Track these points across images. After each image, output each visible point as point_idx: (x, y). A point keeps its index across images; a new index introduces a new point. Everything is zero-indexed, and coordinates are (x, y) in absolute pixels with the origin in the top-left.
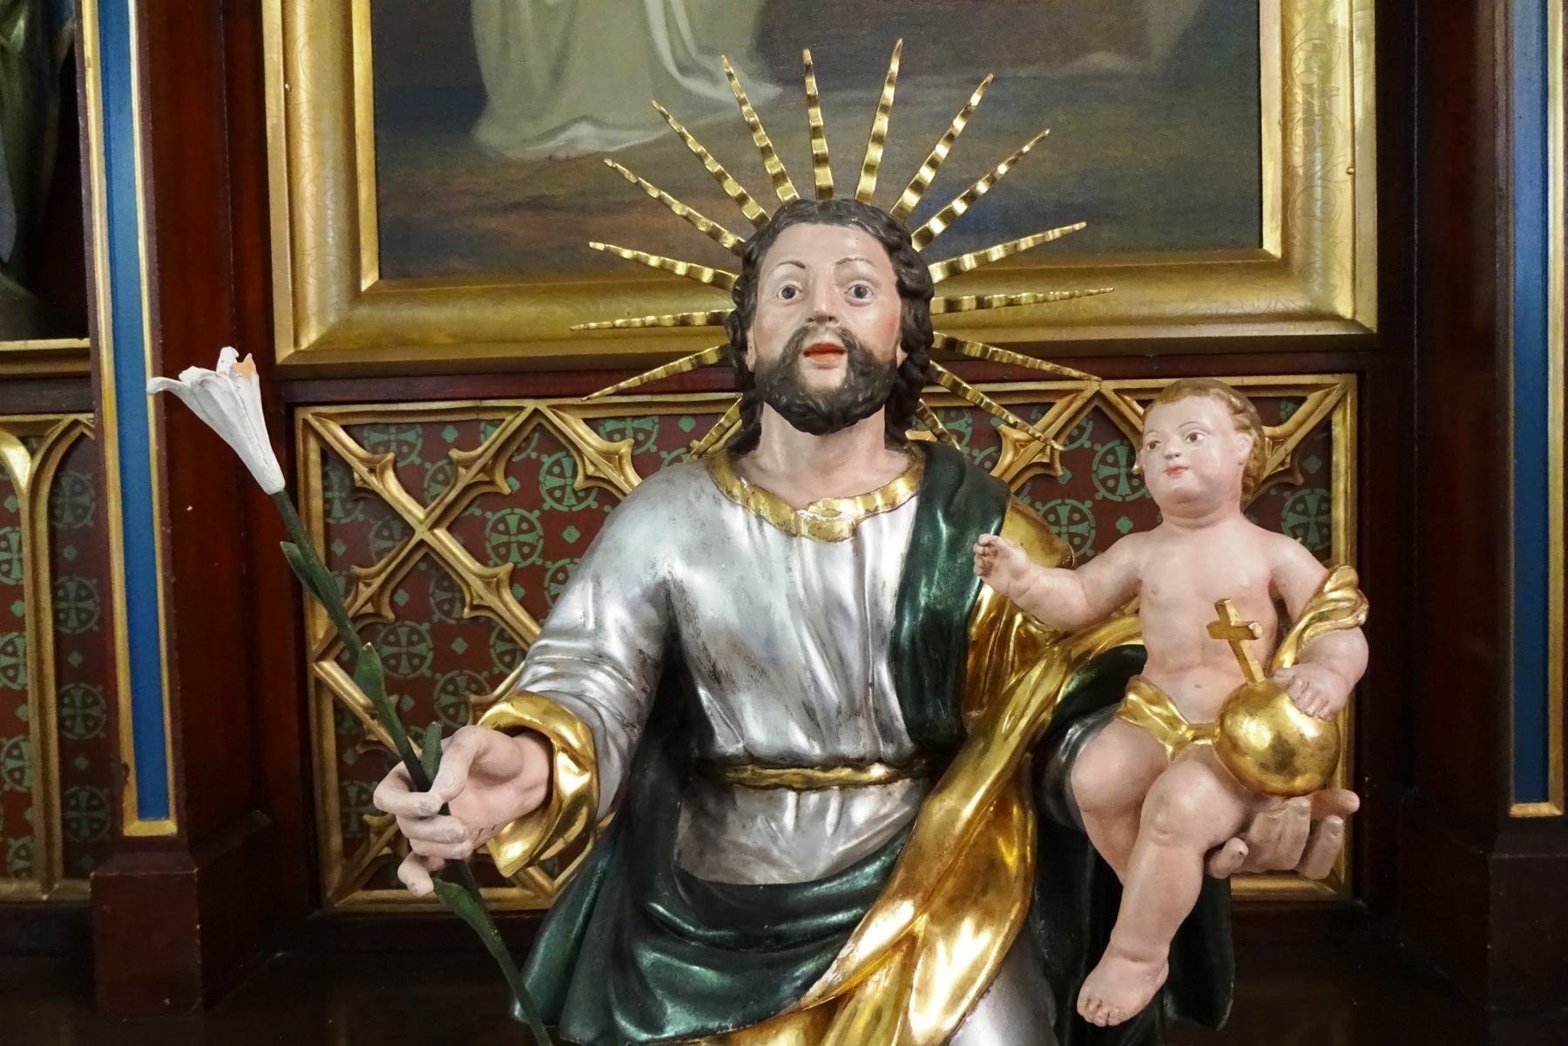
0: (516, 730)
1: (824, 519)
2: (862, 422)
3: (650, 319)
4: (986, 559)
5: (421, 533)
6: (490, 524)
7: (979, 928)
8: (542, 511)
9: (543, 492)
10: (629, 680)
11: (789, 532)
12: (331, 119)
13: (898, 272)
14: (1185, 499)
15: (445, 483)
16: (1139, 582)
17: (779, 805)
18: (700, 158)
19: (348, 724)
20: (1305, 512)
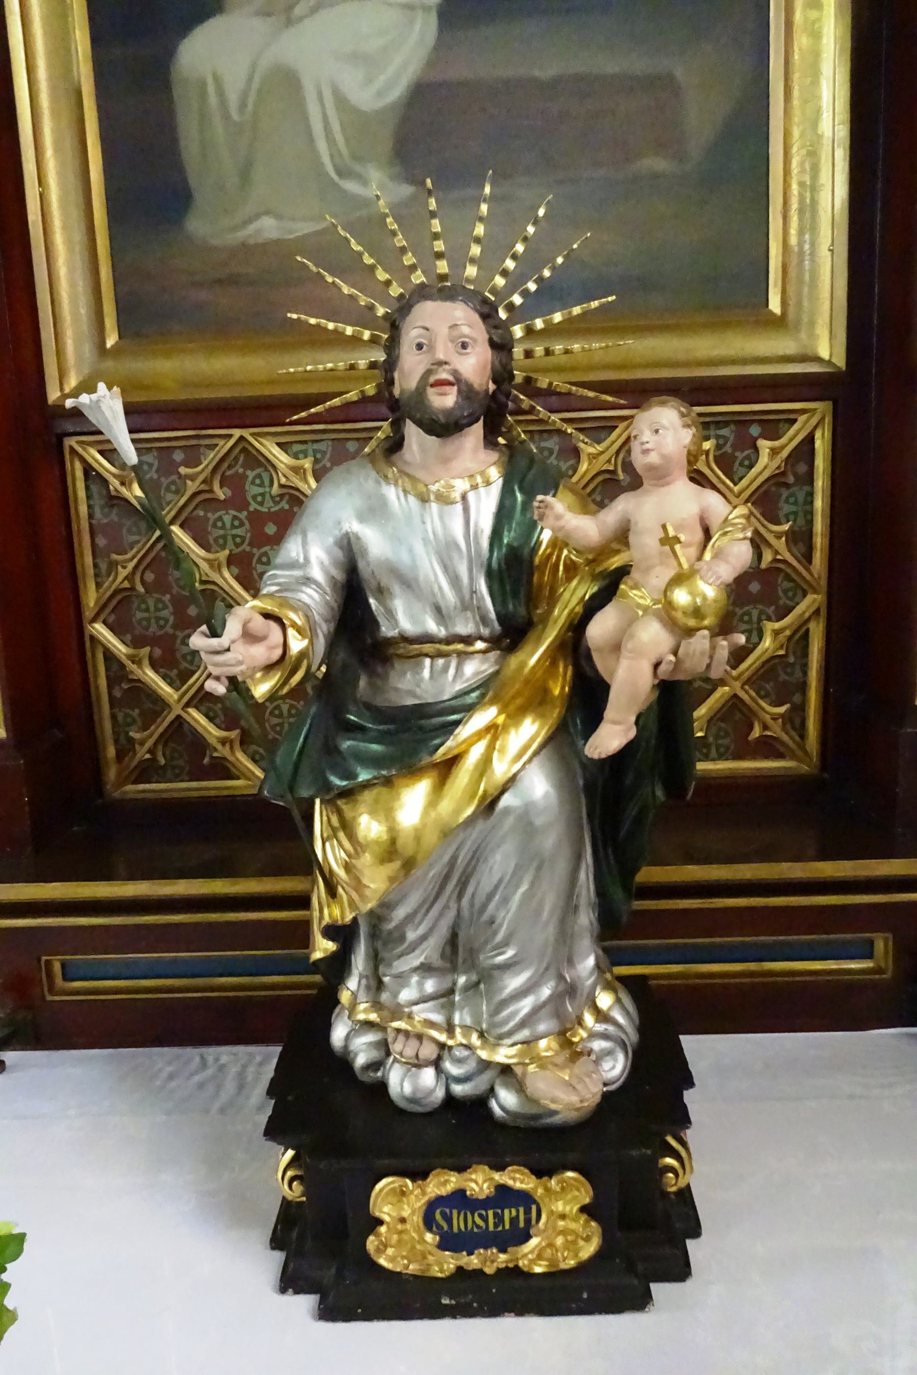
0: (267, 616)
1: (444, 490)
2: (467, 430)
3: (330, 365)
4: (541, 510)
6: (211, 522)
7: (534, 722)
8: (249, 512)
9: (250, 499)
10: (327, 594)
11: (424, 500)
12: (76, 214)
13: (488, 332)
14: (651, 468)
15: (177, 492)
16: (629, 521)
17: (421, 666)
18: (360, 254)
19: (115, 667)
20: (796, 503)
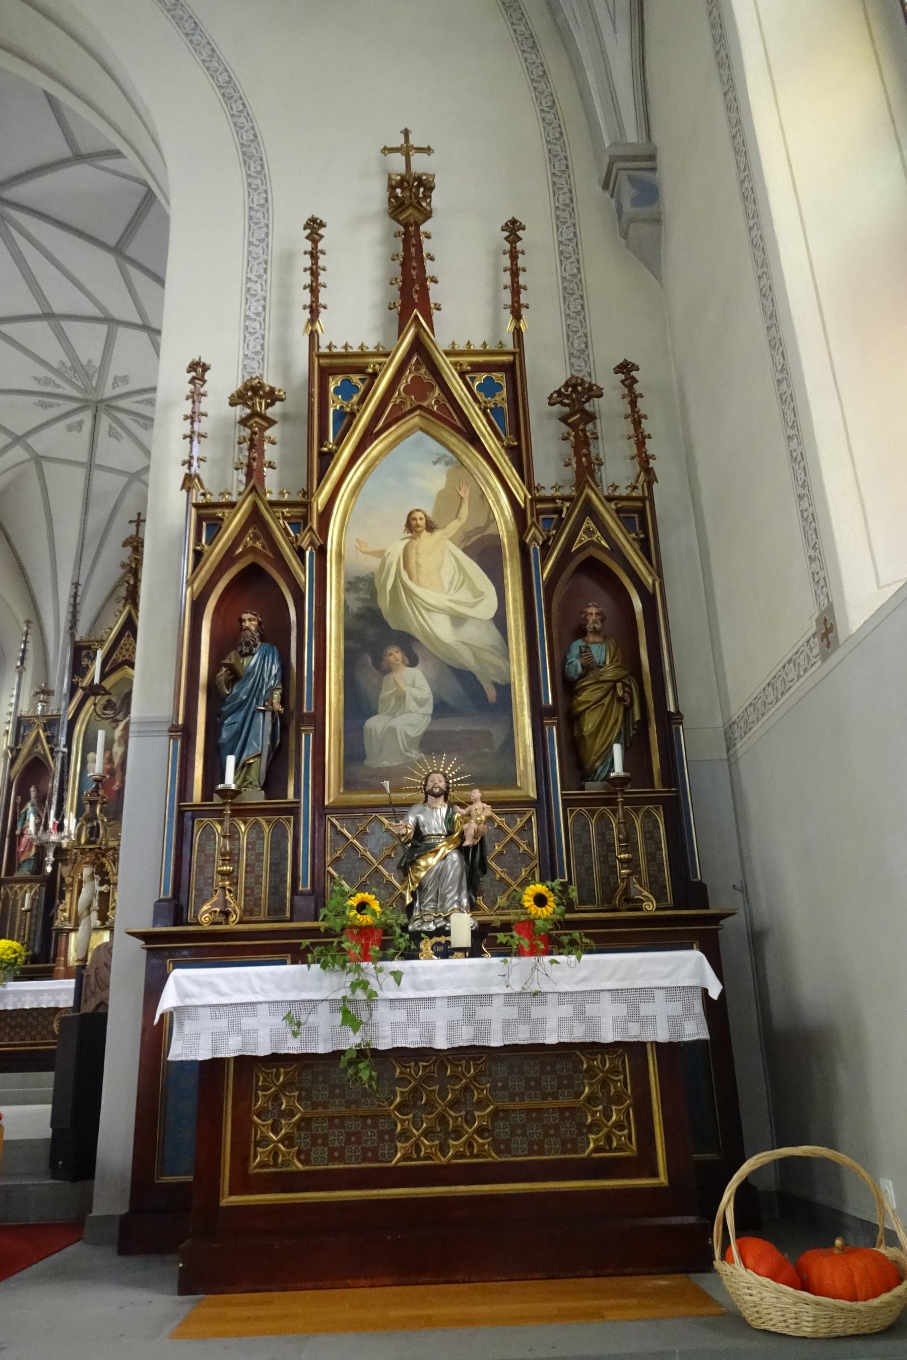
5: (351, 840)
